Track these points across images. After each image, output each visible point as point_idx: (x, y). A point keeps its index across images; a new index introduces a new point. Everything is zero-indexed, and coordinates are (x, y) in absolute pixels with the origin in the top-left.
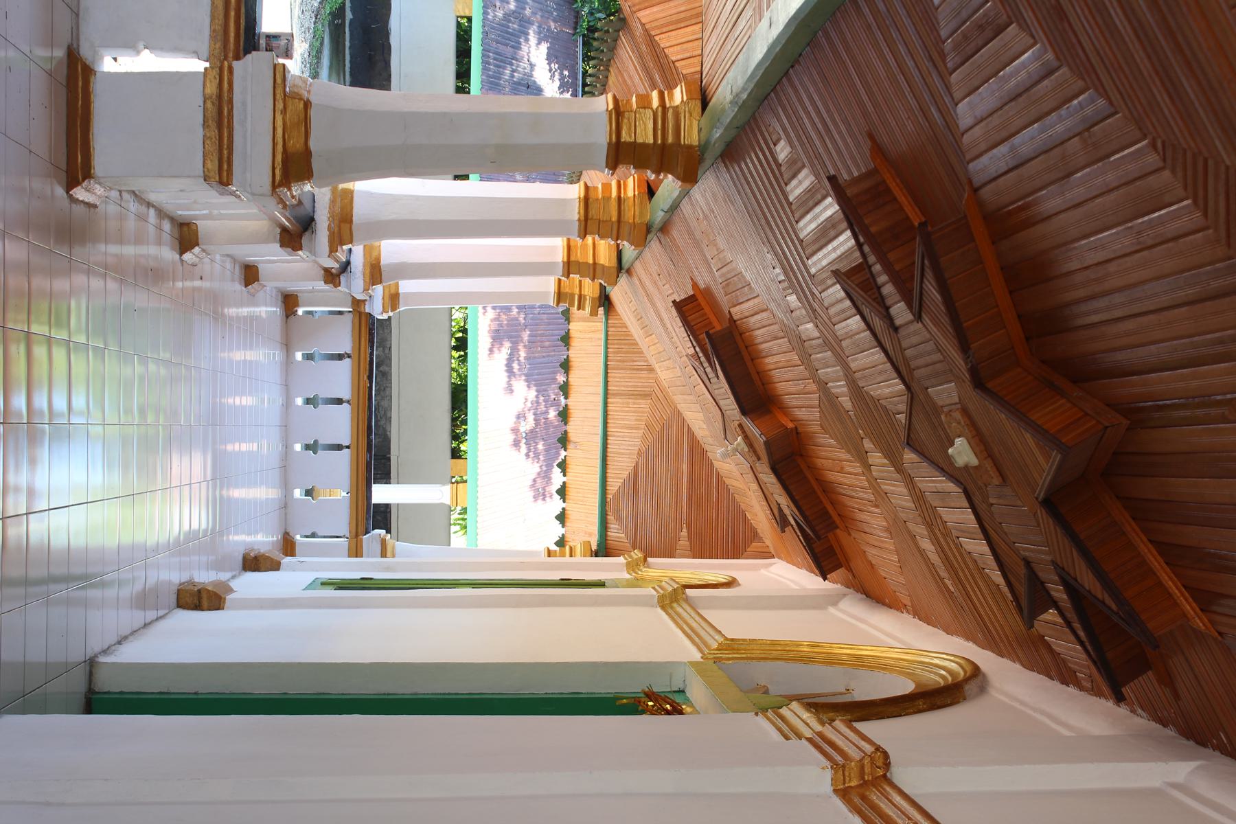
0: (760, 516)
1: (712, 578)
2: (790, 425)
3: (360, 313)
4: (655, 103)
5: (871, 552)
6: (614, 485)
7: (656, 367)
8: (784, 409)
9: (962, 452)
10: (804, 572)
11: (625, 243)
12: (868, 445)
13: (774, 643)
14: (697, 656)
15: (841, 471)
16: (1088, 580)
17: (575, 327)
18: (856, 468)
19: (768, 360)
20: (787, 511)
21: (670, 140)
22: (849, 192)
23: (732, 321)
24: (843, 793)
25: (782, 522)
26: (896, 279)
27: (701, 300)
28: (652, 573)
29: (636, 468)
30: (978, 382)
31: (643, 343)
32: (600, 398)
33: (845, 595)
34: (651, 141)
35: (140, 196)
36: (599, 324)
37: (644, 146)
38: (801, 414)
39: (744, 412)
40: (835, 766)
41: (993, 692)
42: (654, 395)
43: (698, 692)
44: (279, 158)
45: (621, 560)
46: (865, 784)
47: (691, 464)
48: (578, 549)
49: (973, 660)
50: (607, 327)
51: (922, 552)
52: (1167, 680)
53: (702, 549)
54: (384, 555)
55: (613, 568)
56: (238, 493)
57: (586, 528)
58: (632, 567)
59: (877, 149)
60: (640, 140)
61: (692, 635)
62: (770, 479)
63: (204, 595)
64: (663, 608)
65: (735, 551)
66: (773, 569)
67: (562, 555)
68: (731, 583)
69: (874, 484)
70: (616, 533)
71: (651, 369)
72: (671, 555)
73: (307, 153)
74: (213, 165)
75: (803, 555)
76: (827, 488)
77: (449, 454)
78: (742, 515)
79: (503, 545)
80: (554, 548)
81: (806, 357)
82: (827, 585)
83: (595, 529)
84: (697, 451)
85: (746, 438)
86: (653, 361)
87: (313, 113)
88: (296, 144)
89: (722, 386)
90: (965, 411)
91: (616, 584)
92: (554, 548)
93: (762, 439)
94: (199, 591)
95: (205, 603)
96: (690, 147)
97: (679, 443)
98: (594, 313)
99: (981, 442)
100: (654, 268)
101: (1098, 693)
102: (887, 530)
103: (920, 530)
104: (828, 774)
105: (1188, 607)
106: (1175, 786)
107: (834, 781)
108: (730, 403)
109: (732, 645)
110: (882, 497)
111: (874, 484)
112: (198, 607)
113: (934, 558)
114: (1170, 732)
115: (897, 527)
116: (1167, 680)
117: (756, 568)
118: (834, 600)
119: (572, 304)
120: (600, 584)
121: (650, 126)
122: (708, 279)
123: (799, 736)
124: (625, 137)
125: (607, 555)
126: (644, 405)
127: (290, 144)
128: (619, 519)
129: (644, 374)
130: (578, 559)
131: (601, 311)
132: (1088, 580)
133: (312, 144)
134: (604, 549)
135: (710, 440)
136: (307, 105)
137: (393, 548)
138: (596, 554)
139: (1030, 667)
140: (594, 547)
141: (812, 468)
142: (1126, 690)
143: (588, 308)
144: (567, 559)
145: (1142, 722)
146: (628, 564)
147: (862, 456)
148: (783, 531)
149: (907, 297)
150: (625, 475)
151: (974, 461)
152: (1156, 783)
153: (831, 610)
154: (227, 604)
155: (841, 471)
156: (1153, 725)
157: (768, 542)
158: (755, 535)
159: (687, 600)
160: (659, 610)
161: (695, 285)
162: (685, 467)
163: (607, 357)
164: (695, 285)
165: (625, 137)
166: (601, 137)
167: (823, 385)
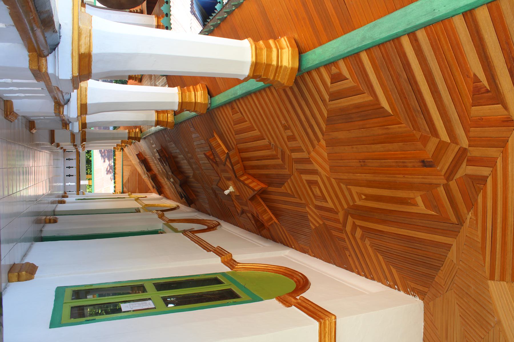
0: (150, 186)
1: (142, 196)
2: (154, 173)
3: (77, 152)
4: (134, 131)
5: (166, 191)
6: (124, 181)
7: (132, 161)
8: (153, 171)
9: (172, 180)
10: (157, 195)
11: (128, 145)
12: (164, 177)
13: (152, 204)
14: (141, 207)
15: (161, 180)
16: (185, 194)
17: (116, 153)
18: (163, 180)
19: (151, 164)
20: (154, 186)
21: (136, 136)
22: (159, 151)
23: (145, 158)
24: (159, 218)
25: (153, 187)
26: (164, 161)
27: (140, 154)
28: (133, 196)
29: (129, 178)
30: (172, 173)
31: (129, 157)
32: (122, 166)
33: (163, 198)
34: (134, 136)
35: (160, 200)
36: (121, 153)
37: (133, 137)
38: (155, 172)
39: (147, 171)
40: (158, 215)
41: (180, 209)
42: (132, 166)
43: (141, 210)
44: (82, 139)
45: (127, 194)
46: (161, 216)
47: (138, 177)
48: (119, 192)
49: (310, 256)
50: (123, 153)
51: (172, 191)
52: (195, 204)
53: (141, 192)
54: (83, 195)
55: (126, 195)
56: (67, 184)
57: (119, 188)
58: (129, 195)
59: (162, 146)
60: (132, 136)
61: (140, 204)
62: (151, 181)
63: (62, 201)
64: (135, 201)
65: (146, 192)
66: (153, 195)
67: (116, 193)
68: (146, 197)
69: (165, 182)
70: (125, 189)
71: (131, 161)
72: (135, 193)
73: (86, 139)
74: (72, 141)
75: (157, 193)
76: (160, 182)
77: (86, 174)
78: (147, 186)
79: (103, 192)
80: (114, 192)
81: (156, 165)
82: (161, 197)
83: (121, 189)
84: (139, 175)
85: (148, 175)
86: (131, 160)
87: (86, 133)
88: (84, 138)
89: (144, 167)
90: (172, 176)
91: (127, 198)
92: (114, 192)
93: (150, 175)
94: (61, 201)
95: (62, 202)
96: (139, 137)
97: (136, 174)
98: (120, 151)
99: (174, 179)
100: (132, 147)
101: (188, 207)
102: (168, 188)
103: (171, 188)
104: (157, 216)
105: (194, 196)
106: (195, 215)
107: (158, 216)
108: (145, 170)
109: (146, 205)
110: (167, 184)
111: (165, 182)
112: (61, 203)
113: (173, 192)
114: (197, 211)
115: (169, 188)
116: (195, 204)
117: (150, 195)
118: (162, 199)
119: (116, 149)
120: (125, 198)
121: (134, 135)
122: (141, 151)
123: (154, 213)
124: (130, 136)
125: (124, 193)
126: (130, 167)
127: (83, 138)
128: (125, 187)
129: (130, 162)
130: (119, 194)
131: (121, 150)
132: (185, 194)
133: (86, 137)
134: (123, 192)
135: (141, 173)
136: (85, 132)
137: (85, 193)
138: (122, 193)
139: (185, 205)
140: (121, 192)
141: (158, 180)
142: (191, 206)
143: (119, 150)
144: (116, 194)
145: (194, 210)
146: (128, 195)
147: (164, 178)
148: (154, 188)
149: (165, 163)
150: (126, 179)
151: (173, 181)
152: (193, 215)
153: (161, 200)
154: (66, 203)
155: (161, 180)
156: (196, 210)
157: (152, 190)
158: (150, 189)
159: (139, 200)
160: (135, 201)
161: (139, 152)
162: (137, 178)
163: (123, 159)
164: (139, 152)
165: (130, 136)
166: (127, 136)
167: (158, 169)
